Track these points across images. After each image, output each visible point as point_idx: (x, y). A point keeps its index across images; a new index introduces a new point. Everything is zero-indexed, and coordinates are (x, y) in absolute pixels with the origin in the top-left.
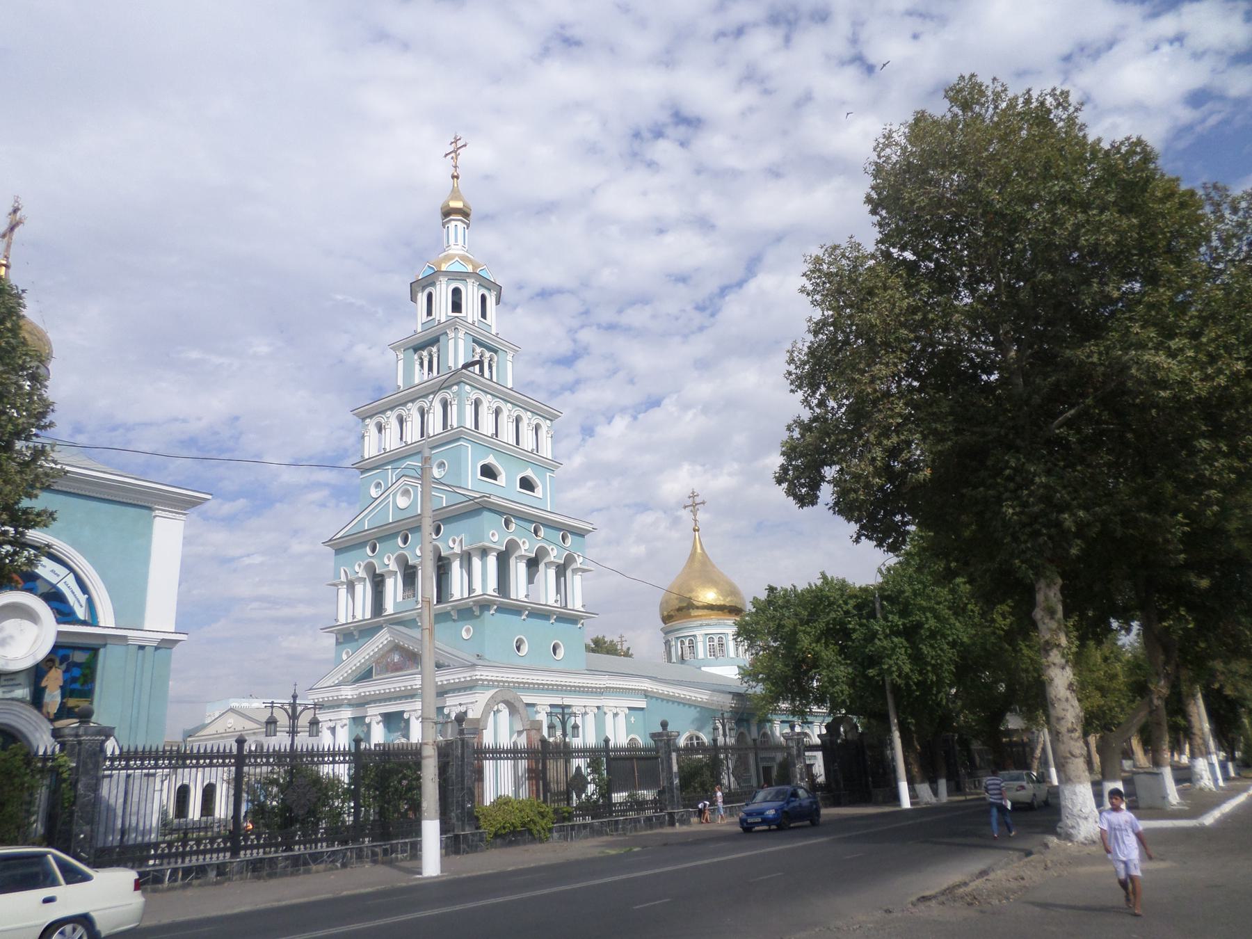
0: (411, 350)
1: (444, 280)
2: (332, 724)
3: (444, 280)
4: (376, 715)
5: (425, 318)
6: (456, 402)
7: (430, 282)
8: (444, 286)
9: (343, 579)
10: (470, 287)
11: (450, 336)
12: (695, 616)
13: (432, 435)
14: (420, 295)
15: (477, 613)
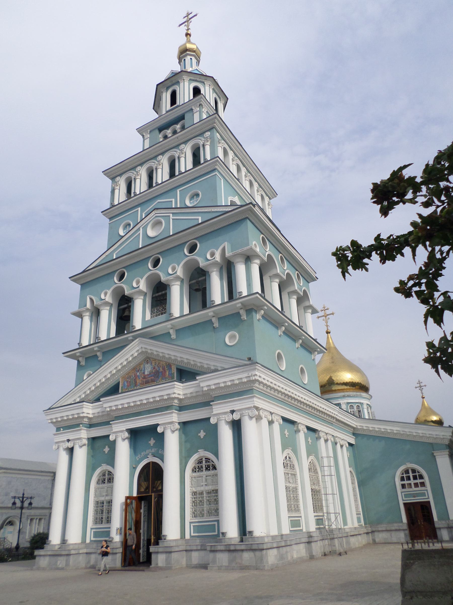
0: (157, 131)
1: (186, 78)
2: (70, 445)
3: (186, 78)
4: (122, 431)
5: (169, 107)
6: (209, 143)
7: (174, 82)
8: (186, 84)
9: (89, 305)
10: (207, 88)
11: (195, 111)
12: (335, 390)
13: (183, 171)
14: (164, 95)
15: (244, 317)
